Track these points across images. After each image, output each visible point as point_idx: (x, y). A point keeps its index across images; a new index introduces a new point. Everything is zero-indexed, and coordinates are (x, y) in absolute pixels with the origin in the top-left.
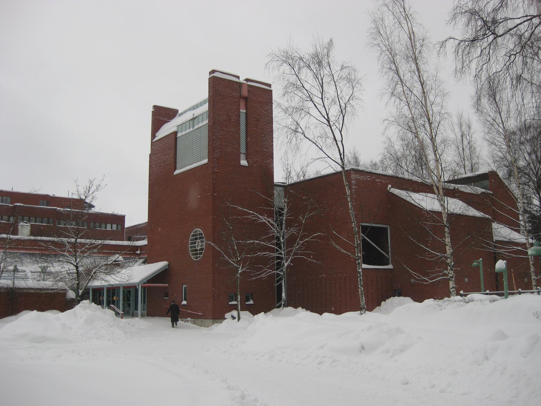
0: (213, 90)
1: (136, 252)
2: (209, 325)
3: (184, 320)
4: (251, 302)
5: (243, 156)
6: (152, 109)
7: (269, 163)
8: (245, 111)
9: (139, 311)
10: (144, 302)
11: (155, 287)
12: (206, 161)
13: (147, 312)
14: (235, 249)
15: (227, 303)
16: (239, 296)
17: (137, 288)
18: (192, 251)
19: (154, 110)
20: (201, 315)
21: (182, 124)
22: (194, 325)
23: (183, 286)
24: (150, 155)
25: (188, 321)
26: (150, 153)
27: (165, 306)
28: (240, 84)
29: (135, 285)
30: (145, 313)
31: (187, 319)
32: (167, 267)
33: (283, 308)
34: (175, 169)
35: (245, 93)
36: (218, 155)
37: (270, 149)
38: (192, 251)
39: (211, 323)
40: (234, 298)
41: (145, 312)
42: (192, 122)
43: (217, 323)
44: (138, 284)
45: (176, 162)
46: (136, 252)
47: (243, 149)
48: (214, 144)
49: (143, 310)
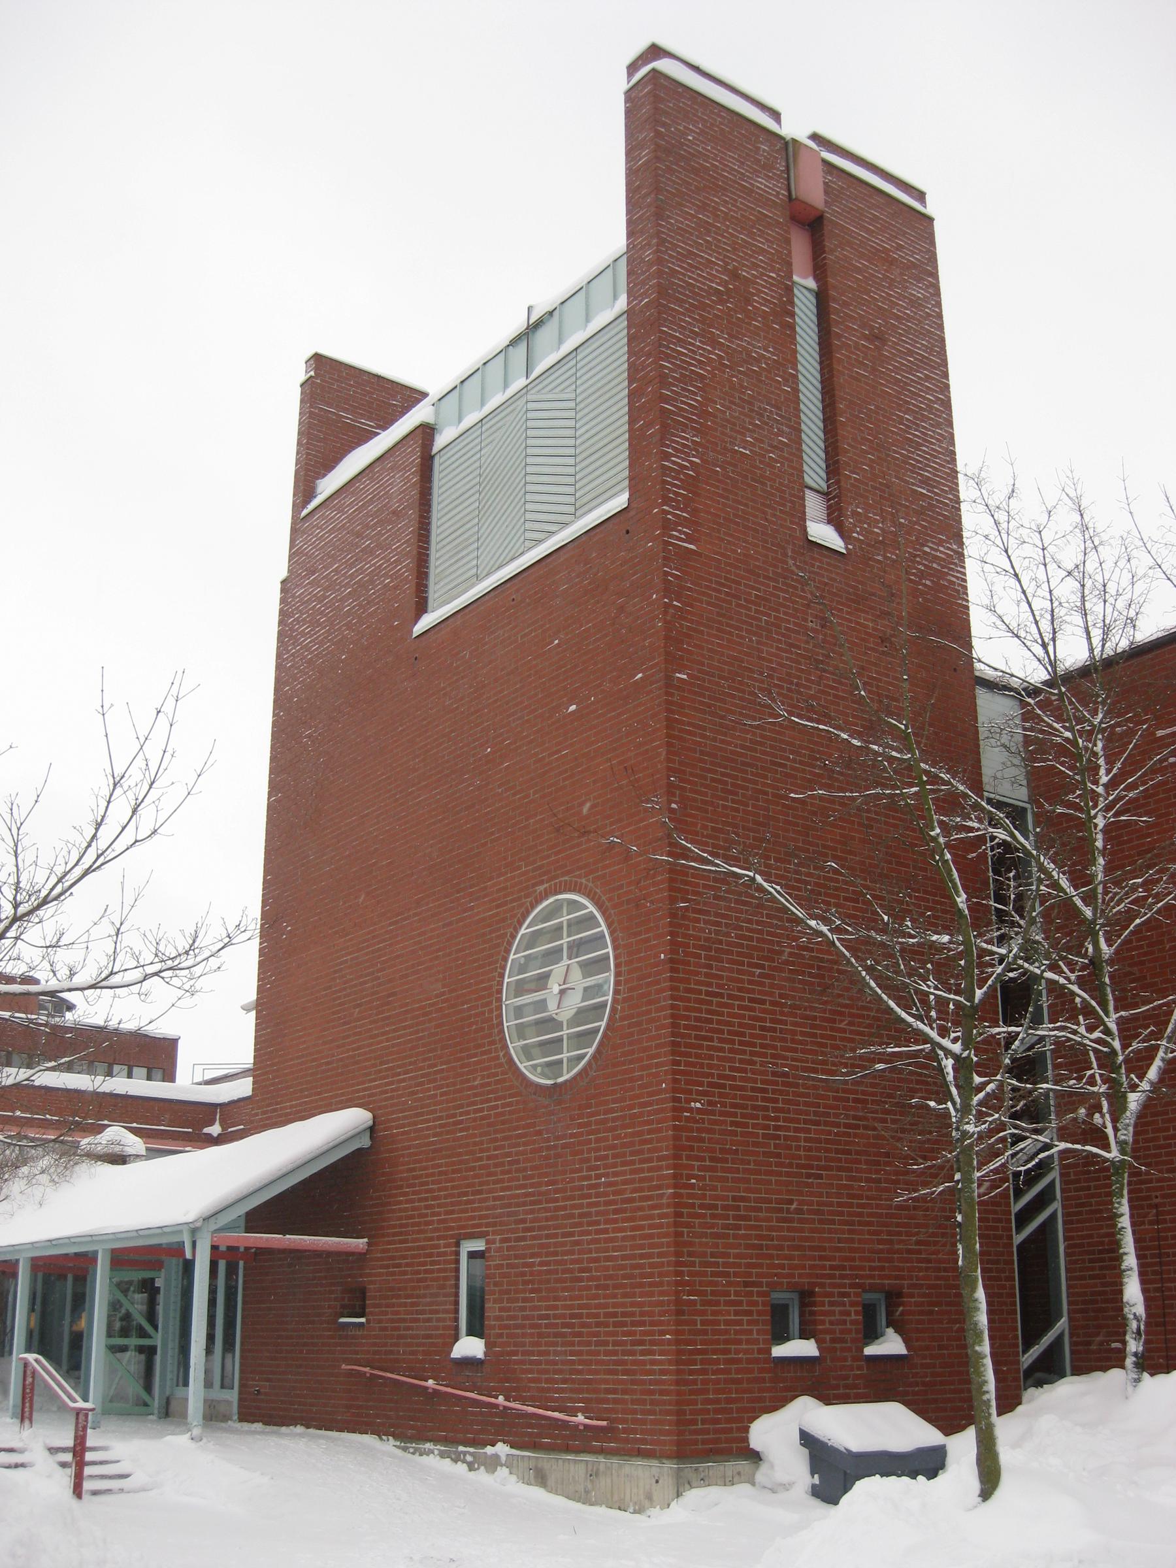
0: (658, 134)
1: (206, 1130)
2: (649, 1497)
3: (469, 1458)
4: (891, 1344)
5: (814, 505)
6: (300, 374)
7: (944, 560)
8: (811, 283)
9: (195, 1395)
10: (229, 1345)
11: (297, 1254)
12: (620, 501)
13: (240, 1400)
14: (960, 911)
15: (760, 1351)
16: (980, 1294)
17: (188, 1256)
18: (521, 1031)
19: (312, 373)
20: (586, 1426)
21: (462, 382)
22: (537, 1493)
23: (458, 1245)
24: (283, 582)
25: (492, 1464)
26: (284, 574)
27: (344, 1366)
28: (788, 147)
29: (175, 1239)
30: (229, 1403)
31: (489, 1450)
32: (366, 1142)
33: (1138, 1380)
34: (422, 608)
35: (812, 189)
36: (691, 462)
37: (946, 492)
38: (521, 1031)
39: (667, 1482)
40: (797, 1321)
41: (233, 1396)
42: (521, 350)
43: (705, 1481)
44: (194, 1231)
45: (426, 575)
46: (206, 1130)
47: (814, 472)
48: (666, 399)
49: (223, 1387)
